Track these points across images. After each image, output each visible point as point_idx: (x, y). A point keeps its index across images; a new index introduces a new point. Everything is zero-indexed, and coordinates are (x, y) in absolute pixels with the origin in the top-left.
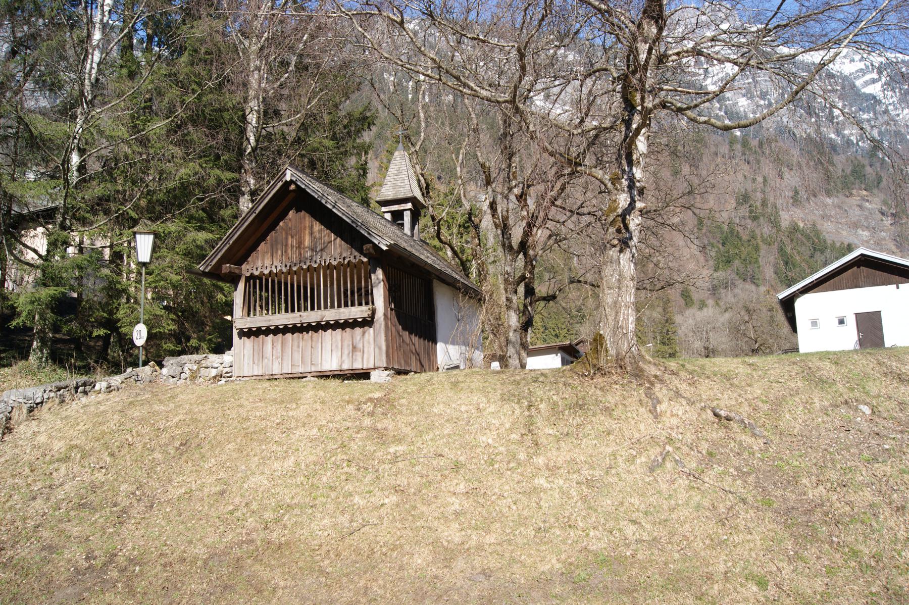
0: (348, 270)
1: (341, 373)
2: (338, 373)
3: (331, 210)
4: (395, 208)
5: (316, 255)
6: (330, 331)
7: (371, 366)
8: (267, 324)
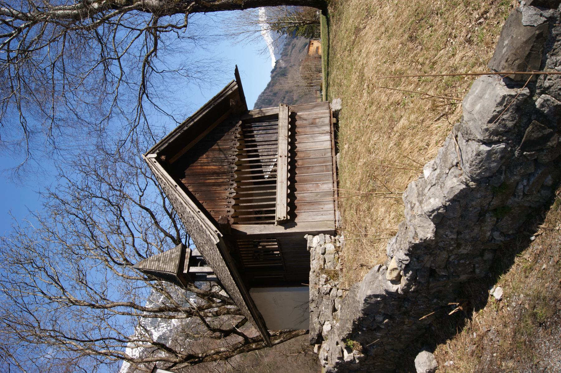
0: (242, 205)
1: (333, 133)
2: (333, 135)
3: (195, 123)
4: (187, 262)
5: (228, 159)
6: (297, 137)
7: (328, 111)
8: (286, 122)
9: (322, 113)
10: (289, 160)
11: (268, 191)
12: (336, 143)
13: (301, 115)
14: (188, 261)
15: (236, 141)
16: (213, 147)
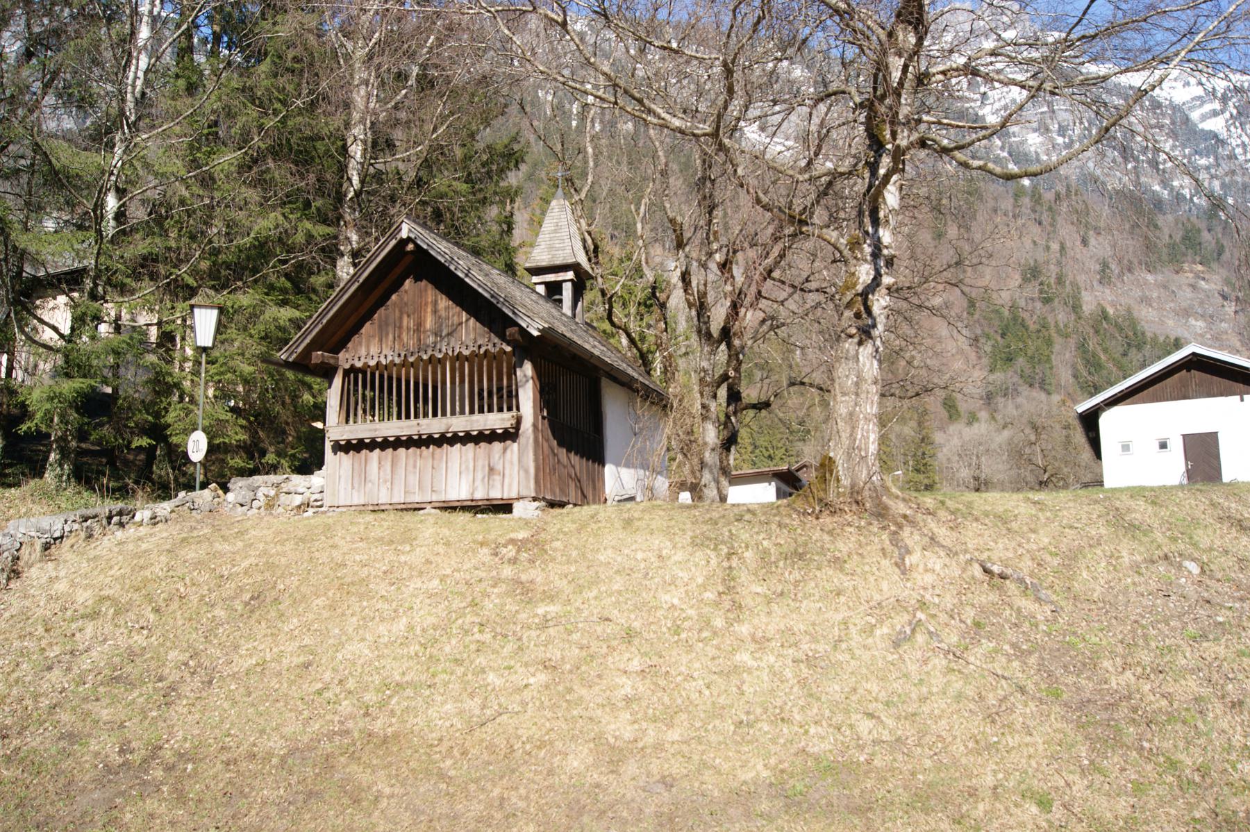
1: (473, 504)
2: (469, 503)
3: (462, 280)
4: (551, 278)
7: (514, 495)
9: (510, 485)
10: (416, 437)
11: (457, 403)
12: (454, 508)
13: (512, 450)
14: (553, 279)
15: (472, 349)
16: (464, 313)
